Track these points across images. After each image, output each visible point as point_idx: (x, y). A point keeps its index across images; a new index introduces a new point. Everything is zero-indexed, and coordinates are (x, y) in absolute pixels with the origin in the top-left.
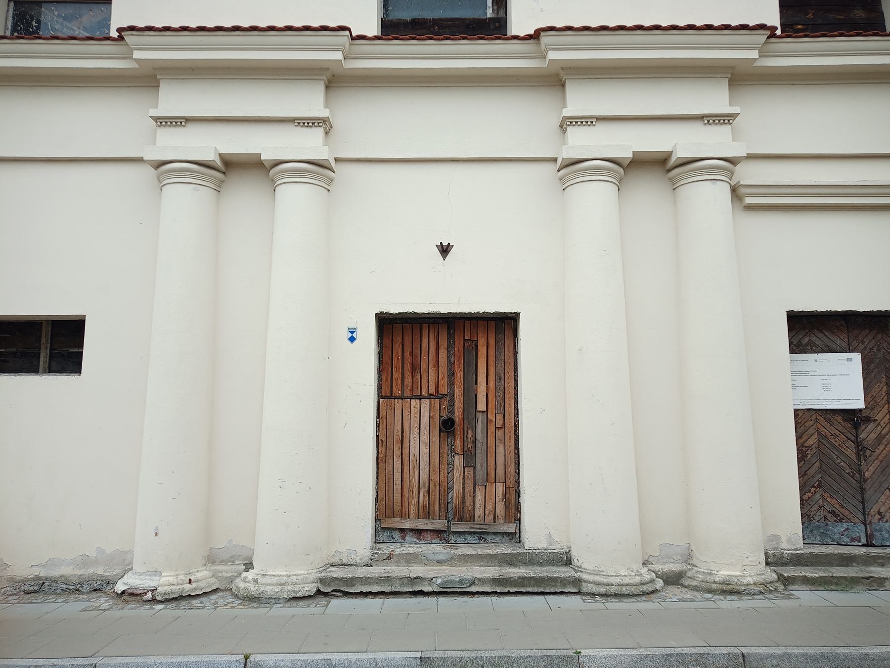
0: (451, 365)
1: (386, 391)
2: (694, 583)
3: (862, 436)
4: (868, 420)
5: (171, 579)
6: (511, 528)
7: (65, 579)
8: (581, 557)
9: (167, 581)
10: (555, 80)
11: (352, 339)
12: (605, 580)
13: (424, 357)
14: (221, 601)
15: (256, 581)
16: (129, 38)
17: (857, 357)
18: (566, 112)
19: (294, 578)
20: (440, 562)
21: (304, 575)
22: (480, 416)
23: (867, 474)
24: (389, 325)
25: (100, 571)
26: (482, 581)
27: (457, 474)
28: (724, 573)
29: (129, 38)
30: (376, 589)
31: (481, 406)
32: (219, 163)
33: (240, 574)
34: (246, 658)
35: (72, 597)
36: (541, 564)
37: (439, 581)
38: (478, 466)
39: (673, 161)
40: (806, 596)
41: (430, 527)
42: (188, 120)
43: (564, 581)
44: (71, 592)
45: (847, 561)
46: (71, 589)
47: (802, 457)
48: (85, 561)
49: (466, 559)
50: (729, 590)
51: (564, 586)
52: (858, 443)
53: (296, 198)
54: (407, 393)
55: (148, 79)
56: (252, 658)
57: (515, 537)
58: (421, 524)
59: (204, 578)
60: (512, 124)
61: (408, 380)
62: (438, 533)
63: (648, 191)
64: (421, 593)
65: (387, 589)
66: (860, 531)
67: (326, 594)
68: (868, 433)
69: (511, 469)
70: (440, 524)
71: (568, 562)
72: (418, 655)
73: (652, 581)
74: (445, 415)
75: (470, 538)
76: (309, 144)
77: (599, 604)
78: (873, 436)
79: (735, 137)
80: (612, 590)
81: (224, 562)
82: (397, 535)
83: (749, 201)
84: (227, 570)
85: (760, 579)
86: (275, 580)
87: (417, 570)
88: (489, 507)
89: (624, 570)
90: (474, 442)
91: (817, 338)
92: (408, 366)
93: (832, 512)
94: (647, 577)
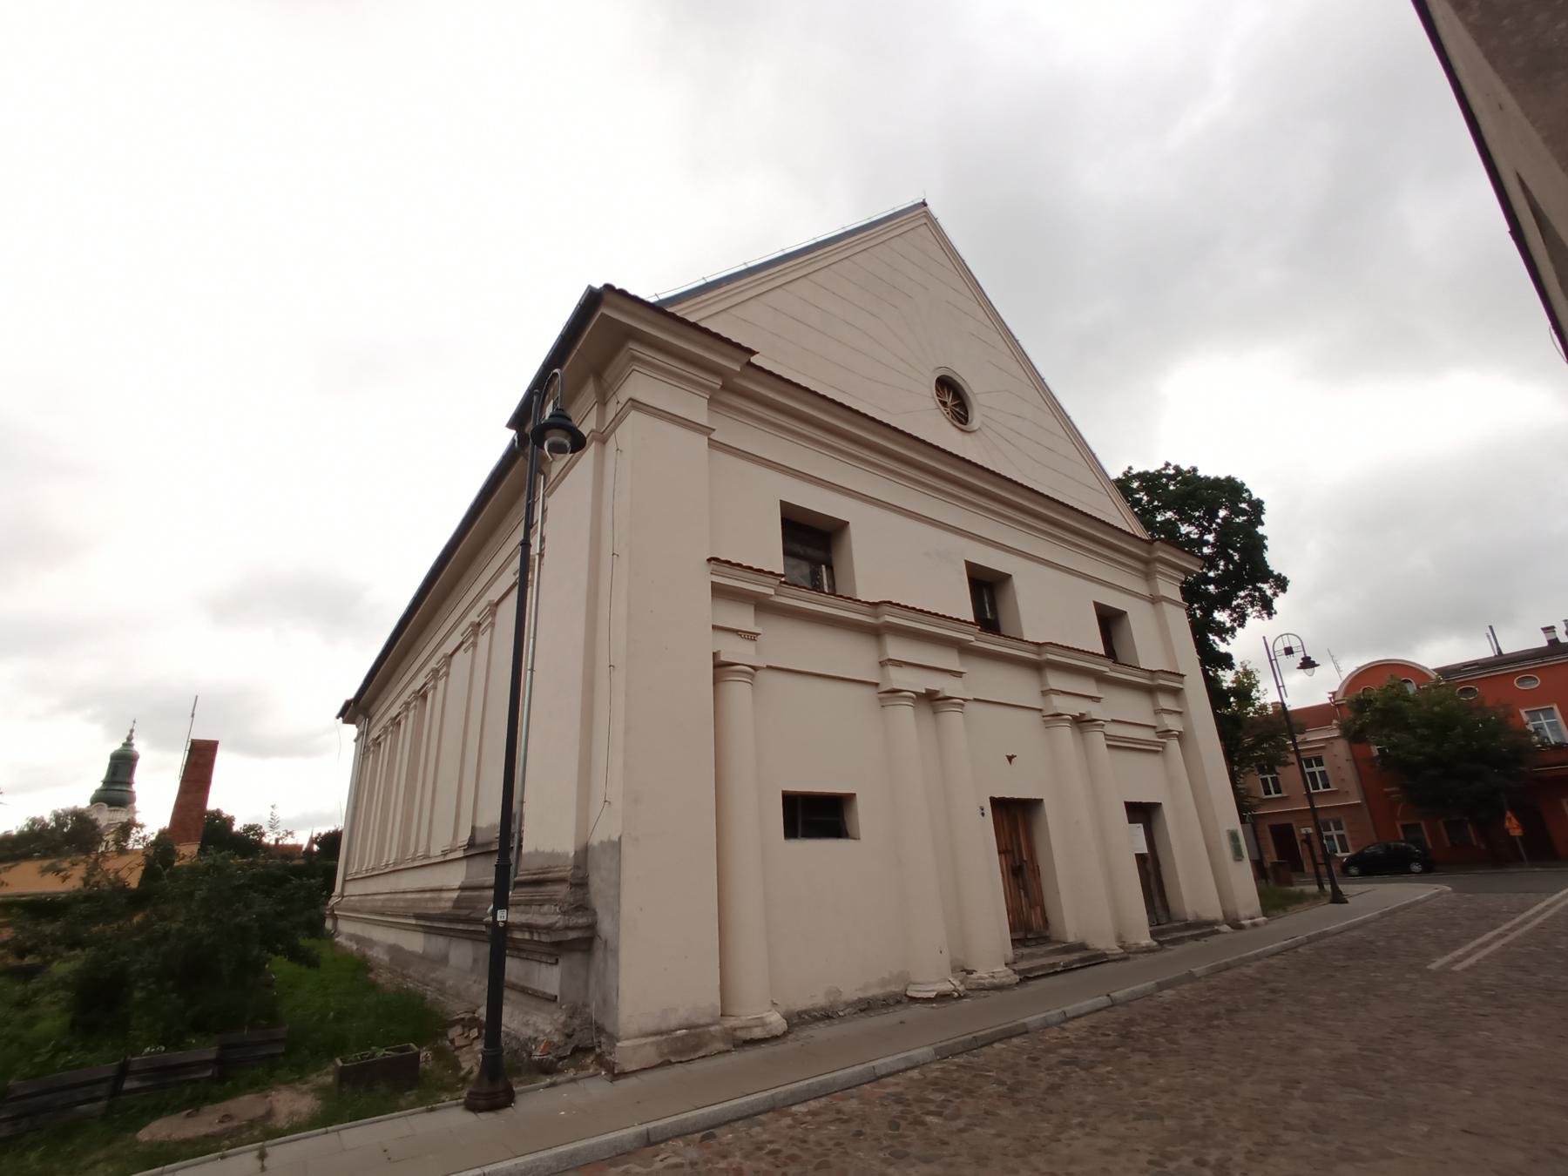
50: (943, 997)
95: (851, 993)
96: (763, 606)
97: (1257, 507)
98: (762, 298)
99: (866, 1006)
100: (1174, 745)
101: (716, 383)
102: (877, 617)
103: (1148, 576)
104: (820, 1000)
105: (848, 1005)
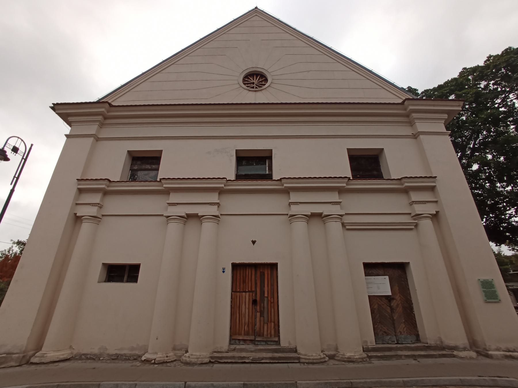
0: (256, 280)
1: (234, 290)
2: (339, 358)
3: (392, 304)
4: (393, 299)
5: (161, 355)
6: (277, 339)
7: (125, 355)
8: (299, 350)
9: (159, 356)
10: (287, 191)
11: (224, 272)
12: (308, 358)
13: (247, 278)
14: (177, 364)
15: (189, 357)
16: (163, 181)
17: (387, 277)
18: (290, 201)
19: (202, 356)
20: (252, 352)
21: (205, 355)
22: (266, 299)
23: (395, 318)
24: (235, 267)
25: (137, 352)
26: (266, 358)
27: (258, 319)
28: (348, 355)
29: (163, 181)
30: (229, 361)
31: (266, 295)
32: (186, 216)
33: (183, 355)
34: (186, 383)
35: (127, 362)
36: (287, 352)
37: (251, 358)
38: (265, 316)
39: (323, 215)
40: (376, 363)
41: (249, 339)
42: (178, 204)
43: (294, 358)
44: (126, 359)
45: (390, 349)
46: (126, 358)
47: (464, 325)
48: (133, 349)
49: (261, 350)
50: (350, 360)
51: (294, 360)
52: (391, 307)
53: (208, 226)
54: (241, 290)
55: (167, 192)
56: (188, 383)
57: (278, 343)
58: (246, 338)
59: (172, 355)
60: (274, 204)
61: (242, 286)
62: (251, 341)
63: (316, 223)
64: (245, 363)
65: (233, 361)
66: (394, 339)
67: (212, 362)
68: (394, 304)
69: (276, 318)
70: (252, 338)
71: (296, 351)
72: (242, 383)
73: (324, 358)
74: (254, 298)
75: (263, 343)
76: (213, 210)
77: (306, 366)
78: (396, 304)
79: (342, 208)
80: (310, 361)
81: (179, 350)
82: (237, 342)
83: (347, 227)
84: (179, 353)
85: (361, 356)
86: (195, 357)
87: (244, 354)
88: (269, 331)
89: (315, 354)
90: (264, 308)
91: (374, 271)
92: (242, 281)
93: (385, 332)
94: (322, 356)
95: (112, 351)
96: (341, 191)
97: (510, 48)
98: (148, 81)
99: (116, 358)
100: (427, 225)
101: (100, 118)
102: (108, 187)
103: (411, 124)
104: (96, 351)
105: (109, 355)
